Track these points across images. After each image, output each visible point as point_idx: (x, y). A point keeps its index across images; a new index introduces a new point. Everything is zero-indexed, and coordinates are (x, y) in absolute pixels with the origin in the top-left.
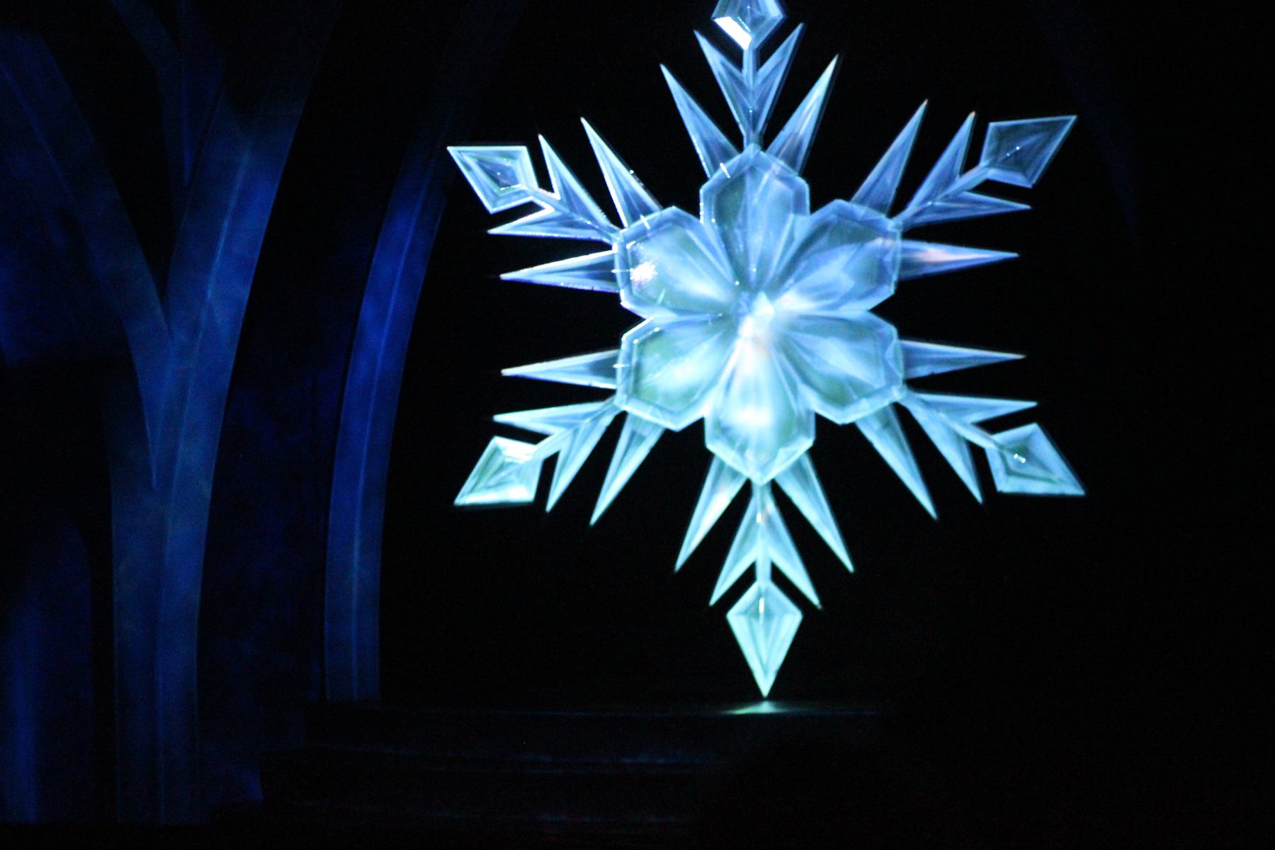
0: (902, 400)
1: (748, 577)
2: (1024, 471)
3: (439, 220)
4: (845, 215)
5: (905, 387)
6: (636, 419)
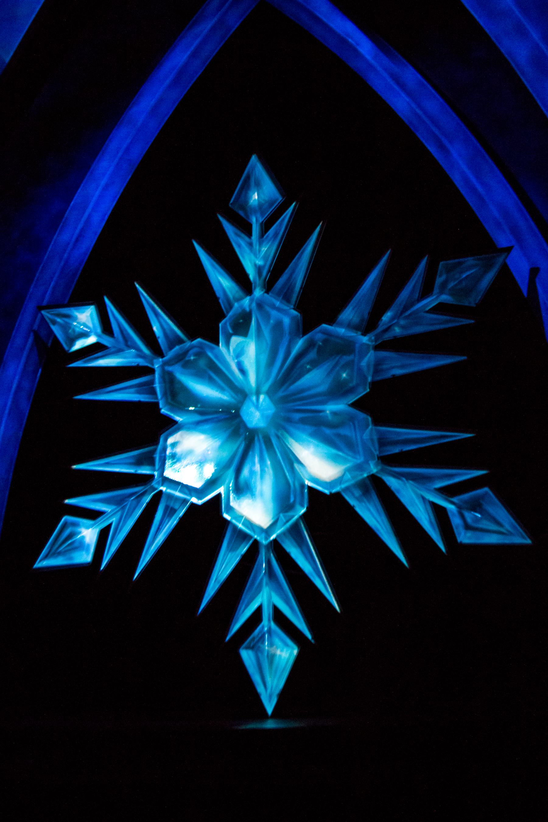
0: (377, 472)
1: (257, 616)
2: (480, 526)
3: (36, 278)
4: (329, 336)
5: (380, 461)
6: (170, 497)
